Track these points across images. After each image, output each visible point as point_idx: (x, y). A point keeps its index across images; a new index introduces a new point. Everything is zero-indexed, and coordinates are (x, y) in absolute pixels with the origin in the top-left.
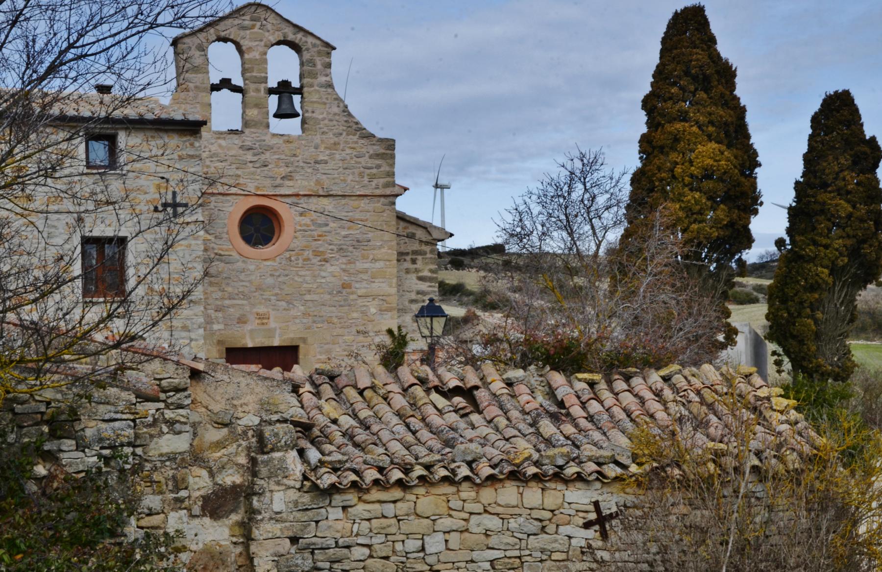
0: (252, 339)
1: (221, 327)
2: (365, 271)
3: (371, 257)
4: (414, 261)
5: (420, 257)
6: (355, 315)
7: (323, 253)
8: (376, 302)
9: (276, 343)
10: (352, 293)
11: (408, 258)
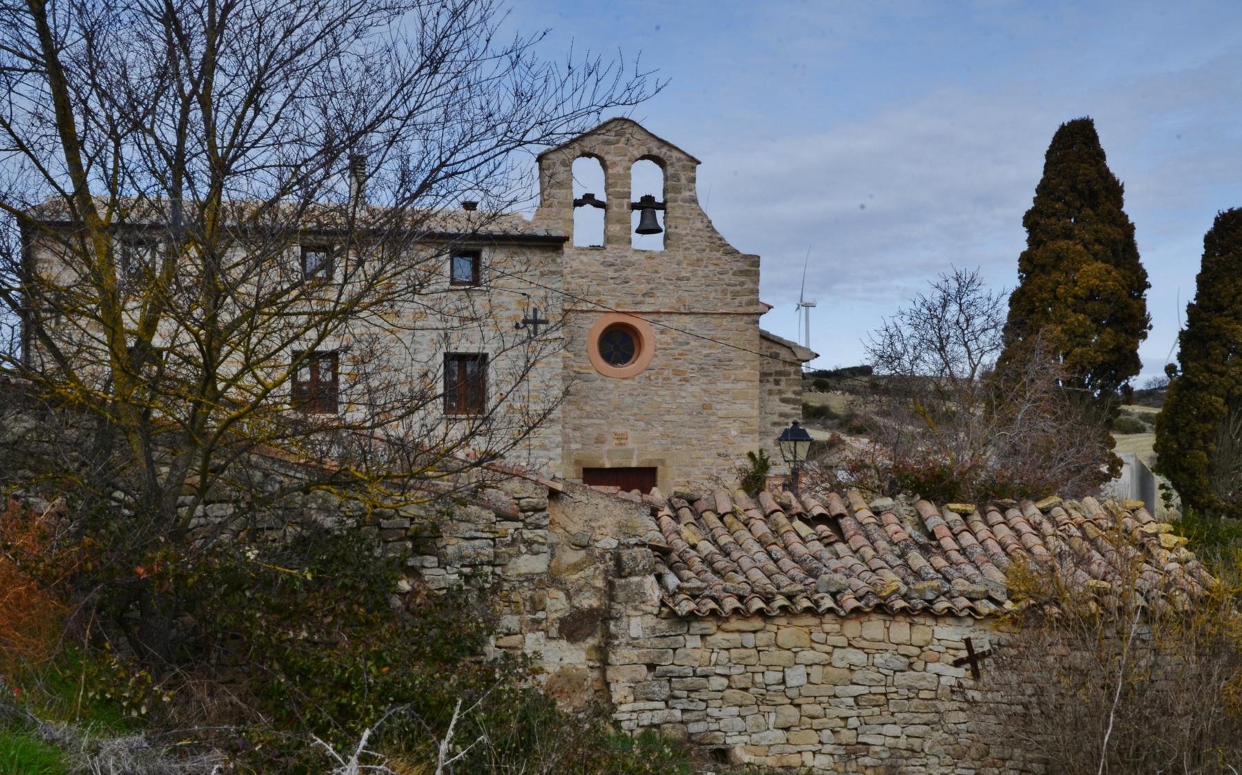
0: (610, 459)
1: (579, 446)
2: (727, 392)
3: (733, 377)
4: (777, 382)
5: (783, 378)
6: (715, 437)
7: (684, 372)
8: (737, 424)
9: (634, 464)
10: (713, 414)
11: (771, 379)
